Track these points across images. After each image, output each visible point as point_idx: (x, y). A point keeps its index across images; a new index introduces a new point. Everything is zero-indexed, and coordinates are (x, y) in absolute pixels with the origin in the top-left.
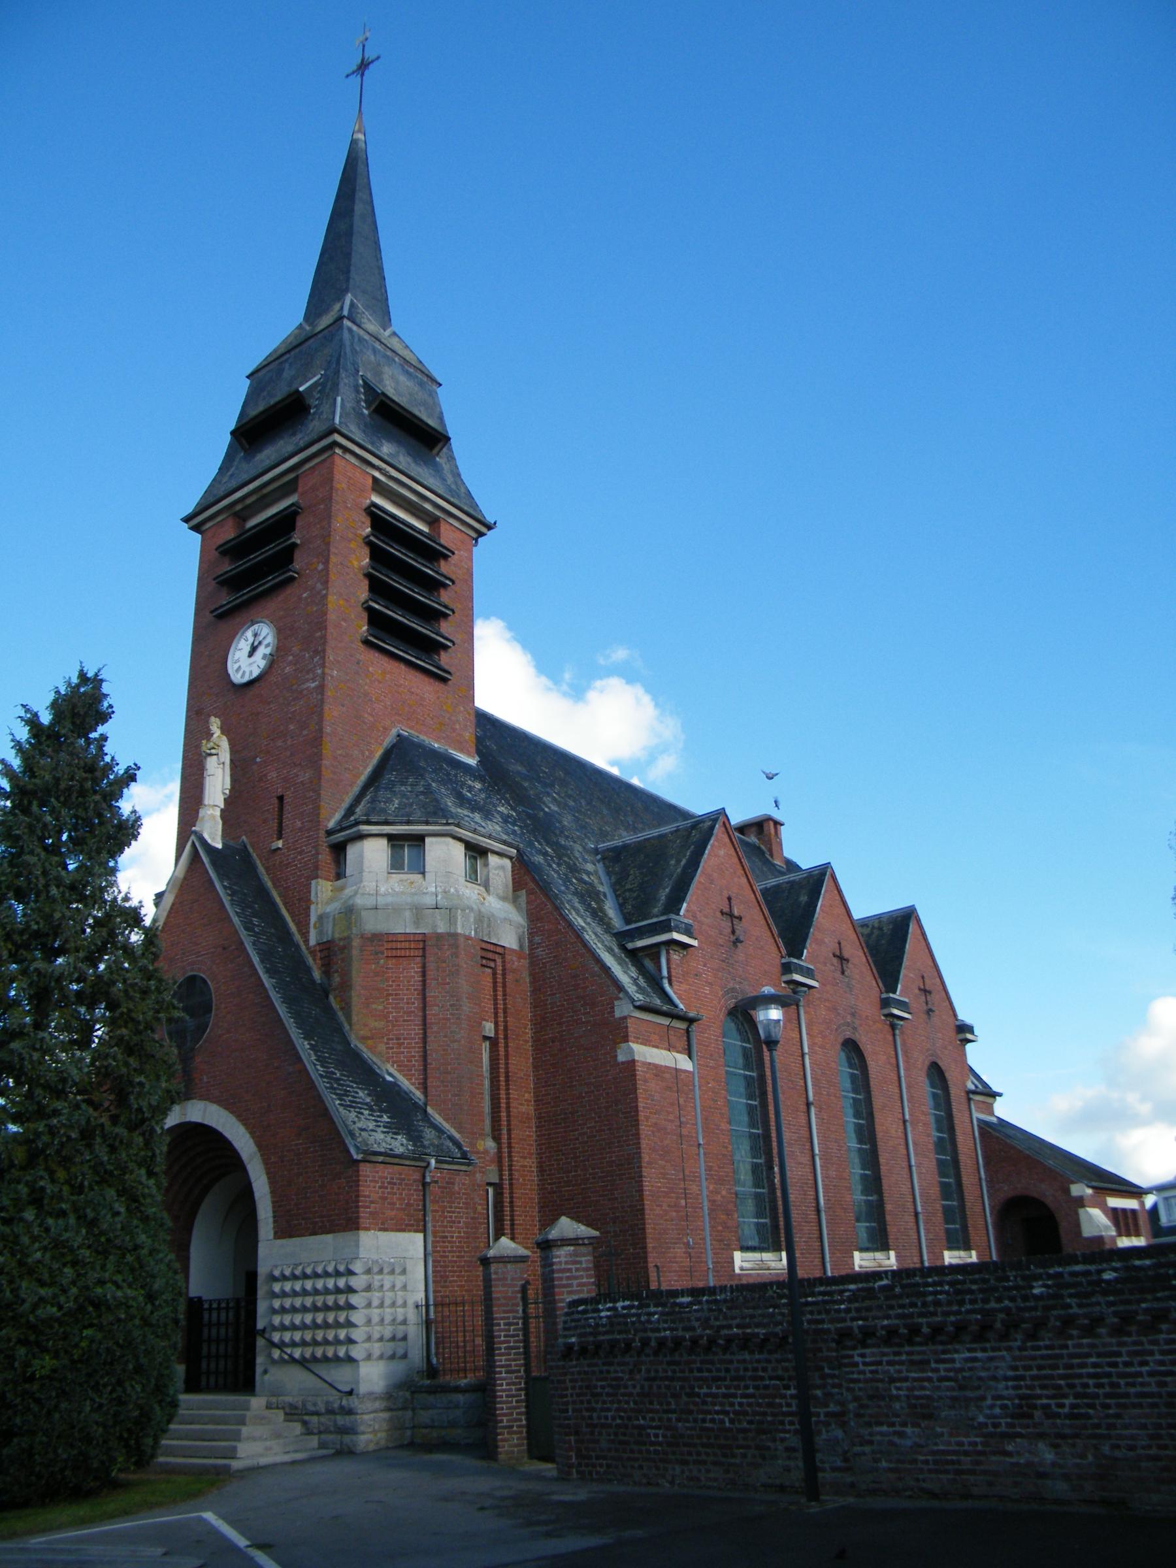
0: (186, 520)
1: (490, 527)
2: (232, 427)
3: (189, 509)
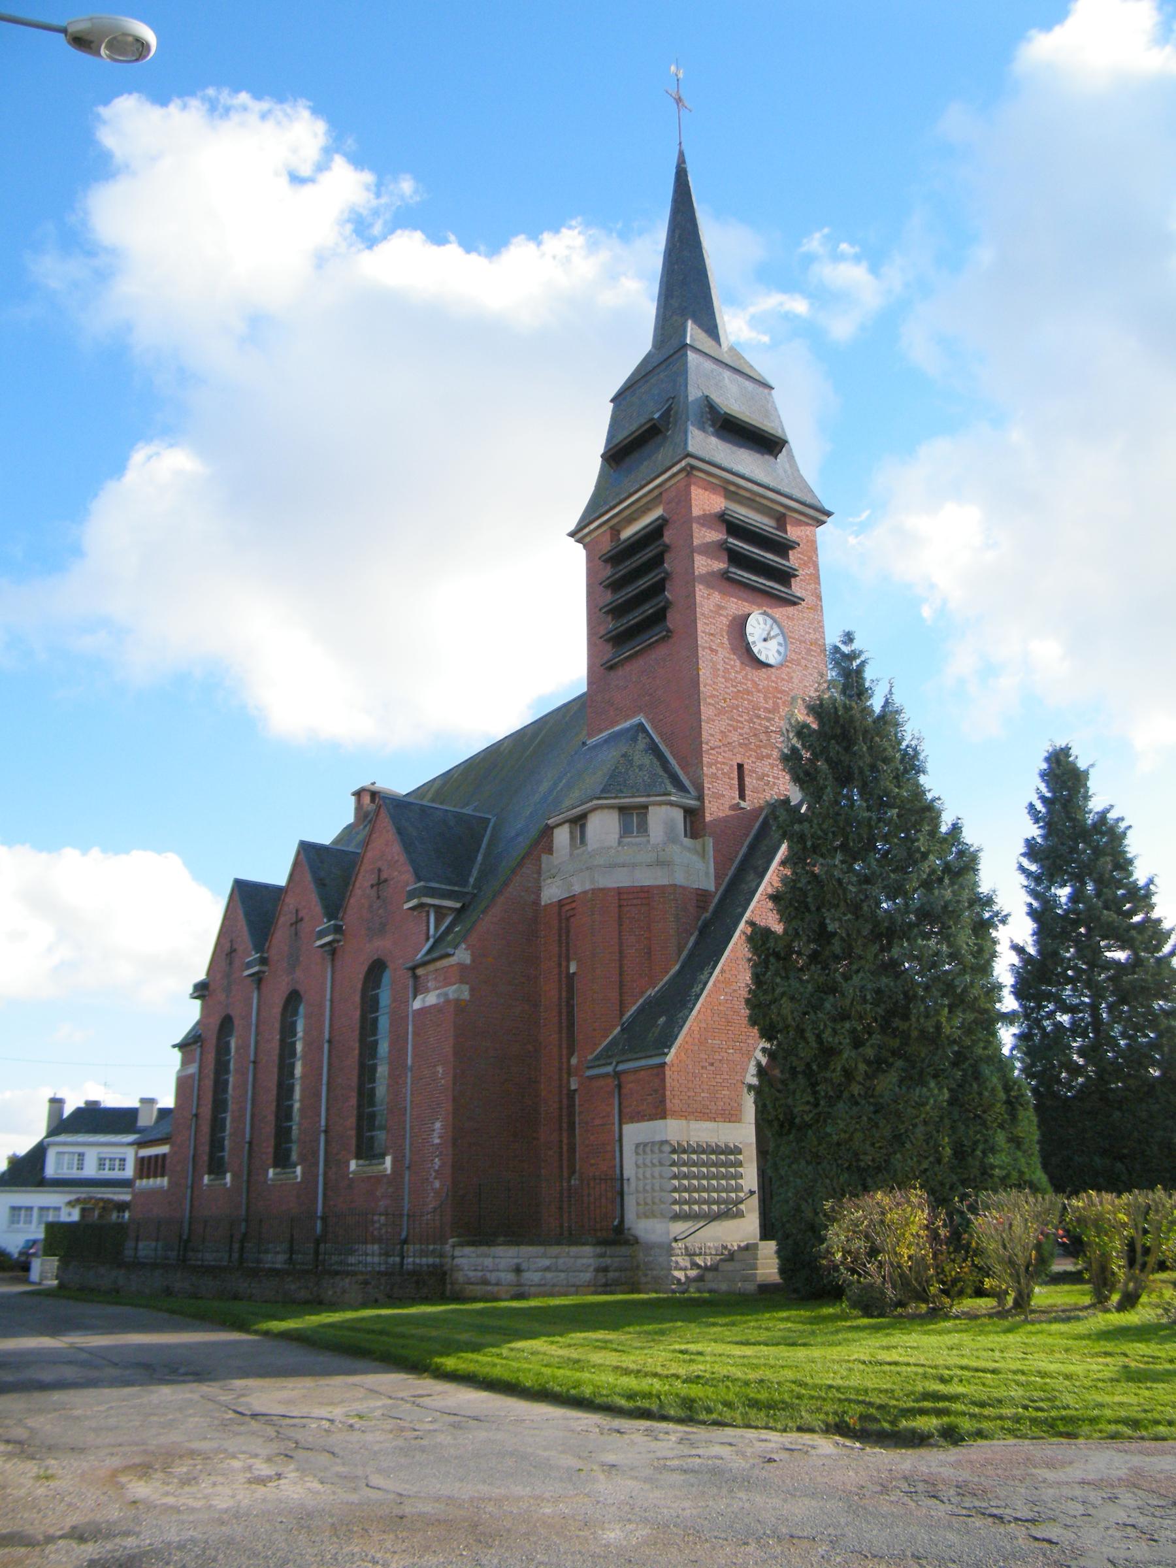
0: (572, 535)
1: (829, 514)
2: (601, 450)
3: (572, 527)
